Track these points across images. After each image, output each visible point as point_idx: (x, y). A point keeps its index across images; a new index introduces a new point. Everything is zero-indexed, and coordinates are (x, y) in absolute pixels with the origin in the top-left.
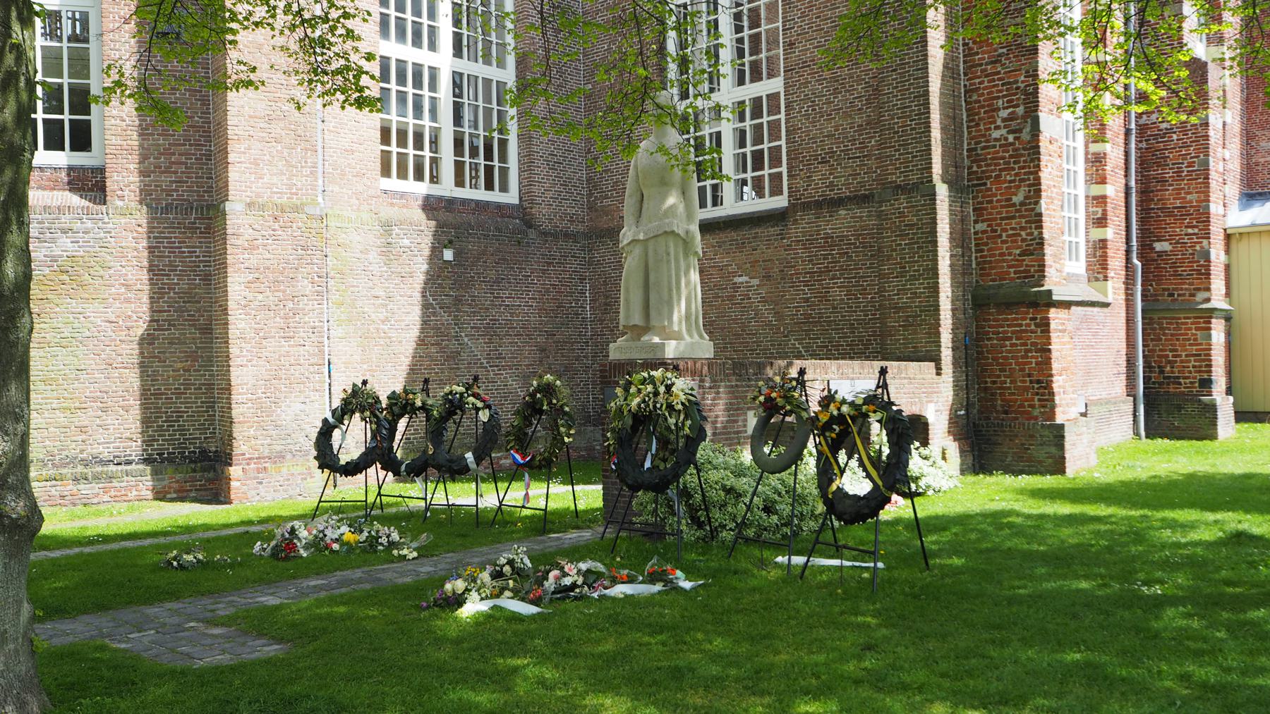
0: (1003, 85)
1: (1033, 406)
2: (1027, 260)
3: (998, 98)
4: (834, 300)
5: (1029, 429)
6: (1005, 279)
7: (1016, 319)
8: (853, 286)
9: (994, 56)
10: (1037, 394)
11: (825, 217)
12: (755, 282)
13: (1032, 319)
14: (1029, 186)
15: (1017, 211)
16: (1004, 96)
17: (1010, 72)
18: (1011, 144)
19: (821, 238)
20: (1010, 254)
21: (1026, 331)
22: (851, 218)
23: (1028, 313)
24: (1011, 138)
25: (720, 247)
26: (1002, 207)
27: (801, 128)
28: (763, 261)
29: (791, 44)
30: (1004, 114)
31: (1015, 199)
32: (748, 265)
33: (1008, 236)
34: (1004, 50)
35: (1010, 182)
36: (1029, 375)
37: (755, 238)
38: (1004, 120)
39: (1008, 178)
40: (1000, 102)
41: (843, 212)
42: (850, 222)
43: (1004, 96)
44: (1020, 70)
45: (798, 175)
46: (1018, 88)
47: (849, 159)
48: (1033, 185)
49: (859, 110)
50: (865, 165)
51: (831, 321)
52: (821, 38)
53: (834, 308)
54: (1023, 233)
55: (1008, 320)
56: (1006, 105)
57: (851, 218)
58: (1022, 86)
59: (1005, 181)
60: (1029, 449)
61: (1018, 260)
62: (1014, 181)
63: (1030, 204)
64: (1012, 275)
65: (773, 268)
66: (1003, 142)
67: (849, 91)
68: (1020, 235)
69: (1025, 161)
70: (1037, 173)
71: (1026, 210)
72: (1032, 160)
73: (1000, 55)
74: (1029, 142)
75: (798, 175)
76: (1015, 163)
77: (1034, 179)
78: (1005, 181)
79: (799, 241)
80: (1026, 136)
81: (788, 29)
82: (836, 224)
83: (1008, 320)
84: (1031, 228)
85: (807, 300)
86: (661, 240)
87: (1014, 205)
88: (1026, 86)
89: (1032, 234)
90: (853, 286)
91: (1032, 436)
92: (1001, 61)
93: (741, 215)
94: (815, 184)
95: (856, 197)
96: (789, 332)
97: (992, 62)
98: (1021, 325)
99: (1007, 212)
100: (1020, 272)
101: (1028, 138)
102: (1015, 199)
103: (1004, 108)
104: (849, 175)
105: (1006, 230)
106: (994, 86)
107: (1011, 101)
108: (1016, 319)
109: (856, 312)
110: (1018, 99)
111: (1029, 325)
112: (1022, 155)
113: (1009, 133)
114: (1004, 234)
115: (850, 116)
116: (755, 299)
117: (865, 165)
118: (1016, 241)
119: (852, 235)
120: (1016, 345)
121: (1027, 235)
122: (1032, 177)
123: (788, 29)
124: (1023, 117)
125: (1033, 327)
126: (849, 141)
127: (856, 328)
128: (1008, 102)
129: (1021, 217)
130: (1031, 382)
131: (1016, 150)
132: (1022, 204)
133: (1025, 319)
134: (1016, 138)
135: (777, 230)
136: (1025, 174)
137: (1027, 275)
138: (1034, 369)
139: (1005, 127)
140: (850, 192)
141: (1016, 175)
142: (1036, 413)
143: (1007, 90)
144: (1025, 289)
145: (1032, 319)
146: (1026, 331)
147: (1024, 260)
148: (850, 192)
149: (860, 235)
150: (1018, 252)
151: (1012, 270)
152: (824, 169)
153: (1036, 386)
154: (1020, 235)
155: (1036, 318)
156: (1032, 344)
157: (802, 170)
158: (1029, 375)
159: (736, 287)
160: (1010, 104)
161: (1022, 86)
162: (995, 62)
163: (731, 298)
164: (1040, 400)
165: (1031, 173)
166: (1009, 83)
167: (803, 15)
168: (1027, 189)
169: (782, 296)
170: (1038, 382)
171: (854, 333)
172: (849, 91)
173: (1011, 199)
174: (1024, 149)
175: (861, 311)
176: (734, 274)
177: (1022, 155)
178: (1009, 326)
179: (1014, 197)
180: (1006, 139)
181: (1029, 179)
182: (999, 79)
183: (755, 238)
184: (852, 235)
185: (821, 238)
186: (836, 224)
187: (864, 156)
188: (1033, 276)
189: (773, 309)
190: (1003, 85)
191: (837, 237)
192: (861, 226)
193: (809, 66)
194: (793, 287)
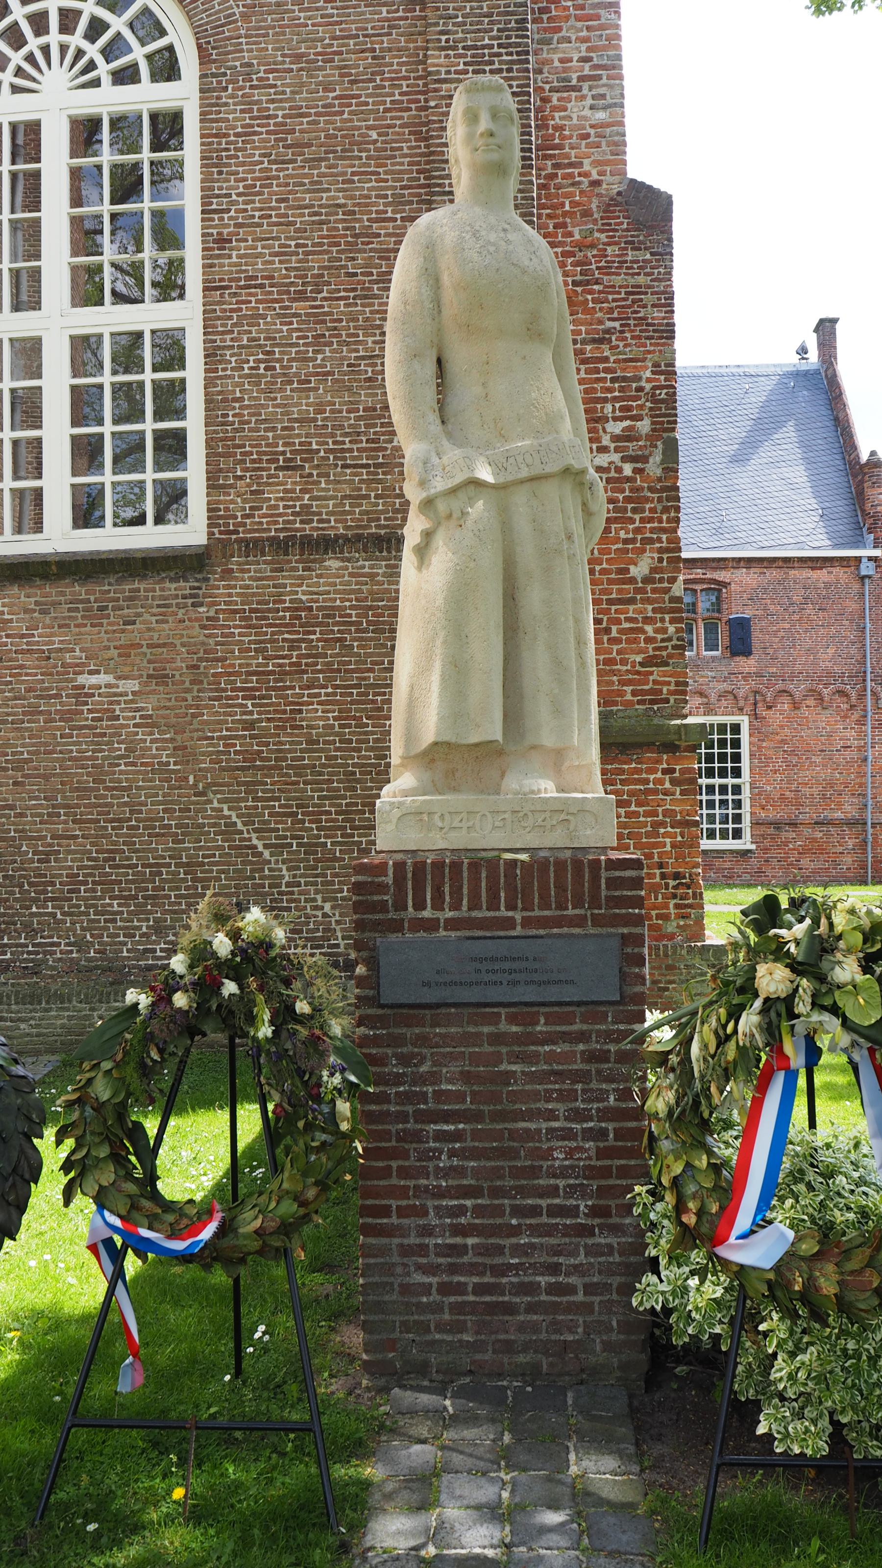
0: (613, 380)
1: (666, 917)
2: (656, 674)
3: (605, 400)
4: (309, 727)
5: (666, 955)
6: (615, 703)
7: (638, 771)
8: (352, 702)
9: (597, 332)
10: (674, 896)
11: (296, 569)
12: (132, 685)
13: (665, 772)
14: (661, 550)
15: (637, 591)
16: (615, 399)
17: (626, 360)
18: (628, 479)
19: (285, 610)
20: (624, 662)
21: (655, 792)
22: (351, 575)
23: (659, 761)
24: (628, 469)
25: (43, 612)
26: (610, 582)
27: (241, 400)
28: (149, 646)
29: (222, 241)
30: (616, 428)
31: (634, 571)
32: (114, 653)
33: (621, 631)
34: (617, 324)
35: (626, 541)
36: (661, 866)
37: (131, 599)
38: (615, 438)
39: (622, 534)
40: (609, 408)
41: (334, 564)
42: (349, 583)
43: (615, 399)
44: (644, 360)
45: (231, 486)
46: (640, 389)
47: (345, 466)
48: (667, 550)
49: (369, 379)
50: (379, 481)
51: (305, 767)
52: (287, 238)
53: (310, 742)
54: (649, 629)
55: (622, 772)
56: (618, 414)
57: (351, 575)
58: (648, 386)
59: (617, 540)
60: (667, 989)
61: (638, 673)
62: (633, 541)
63: (661, 580)
64: (629, 697)
65: (173, 660)
66: (613, 474)
67: (348, 344)
68: (642, 631)
69: (652, 510)
70: (675, 530)
71: (654, 591)
72: (666, 510)
73: (608, 331)
74: (659, 480)
75: (231, 486)
76: (635, 511)
77: (669, 541)
78: (617, 540)
79: (235, 612)
80: (654, 468)
81: (215, 211)
82: (318, 585)
83: (622, 772)
84: (662, 620)
85: (250, 725)
86: (551, 490)
87: (633, 580)
88: (654, 388)
89: (664, 630)
90: (352, 702)
91: (671, 968)
92: (610, 341)
93: (91, 553)
94: (270, 507)
95: (359, 538)
96: (208, 786)
97: (594, 341)
98: (646, 781)
99: (619, 591)
100: (643, 692)
101: (659, 472)
102: (634, 571)
103: (615, 419)
104: (344, 497)
105: (618, 622)
106: (598, 380)
107: (629, 409)
108: (638, 771)
109: (359, 750)
110: (641, 407)
111: (661, 782)
112: (647, 500)
113: (624, 459)
114: (614, 629)
115: (349, 389)
116: (127, 719)
117: (379, 481)
118: (636, 641)
119: (351, 607)
120: (636, 814)
121: (656, 631)
122: (664, 537)
123: (215, 211)
124: (648, 437)
125: (667, 785)
126: (346, 435)
127: (358, 781)
128: (622, 409)
129: (643, 601)
130: (663, 876)
131: (639, 489)
132: (646, 580)
133: (653, 771)
134: (636, 471)
135: (185, 586)
136: (652, 530)
137: (656, 698)
138: (668, 854)
139: (617, 450)
140: (347, 528)
141: (637, 531)
142: (671, 927)
143: (622, 389)
144: (656, 721)
145: (665, 772)
146: (655, 792)
147: (652, 673)
148: (347, 528)
149: (370, 608)
150: (639, 658)
151: (629, 689)
152: (292, 481)
153: (672, 883)
154: (643, 631)
155: (673, 771)
156: (666, 813)
157: (241, 478)
158: (661, 866)
159: (81, 694)
160: (626, 413)
161: (648, 386)
162: (601, 341)
163: (68, 716)
164: (677, 906)
165: (664, 530)
166: (624, 379)
167: (249, 192)
168: (656, 555)
169: (194, 716)
170: (677, 876)
171: (354, 789)
172: (348, 344)
173: (627, 571)
174: (650, 489)
175: (372, 749)
176: (79, 668)
177: (647, 500)
178: (623, 782)
179: (632, 568)
180: (619, 470)
181: (659, 540)
182: (607, 370)
183: (131, 599)
184: (351, 607)
185: (285, 610)
186: (318, 585)
187: (377, 466)
188: (667, 701)
189: (172, 740)
190: (613, 380)
191: (319, 609)
192: (371, 592)
193: (262, 286)
194: (218, 699)
